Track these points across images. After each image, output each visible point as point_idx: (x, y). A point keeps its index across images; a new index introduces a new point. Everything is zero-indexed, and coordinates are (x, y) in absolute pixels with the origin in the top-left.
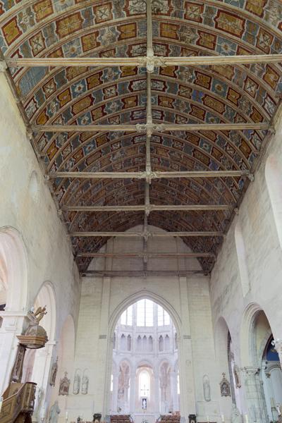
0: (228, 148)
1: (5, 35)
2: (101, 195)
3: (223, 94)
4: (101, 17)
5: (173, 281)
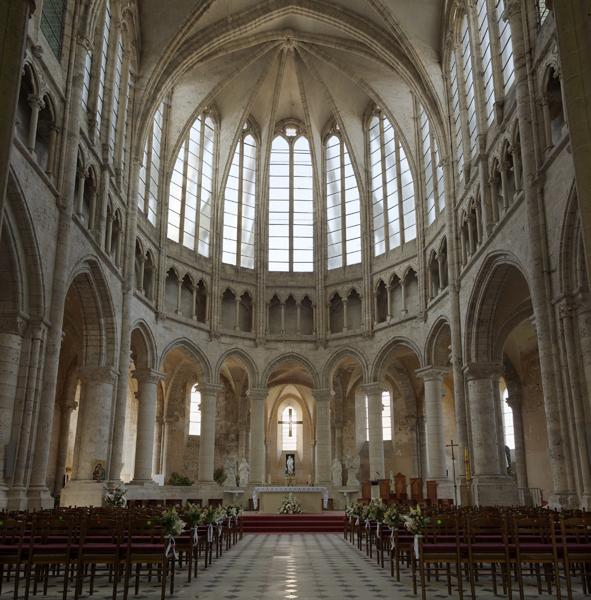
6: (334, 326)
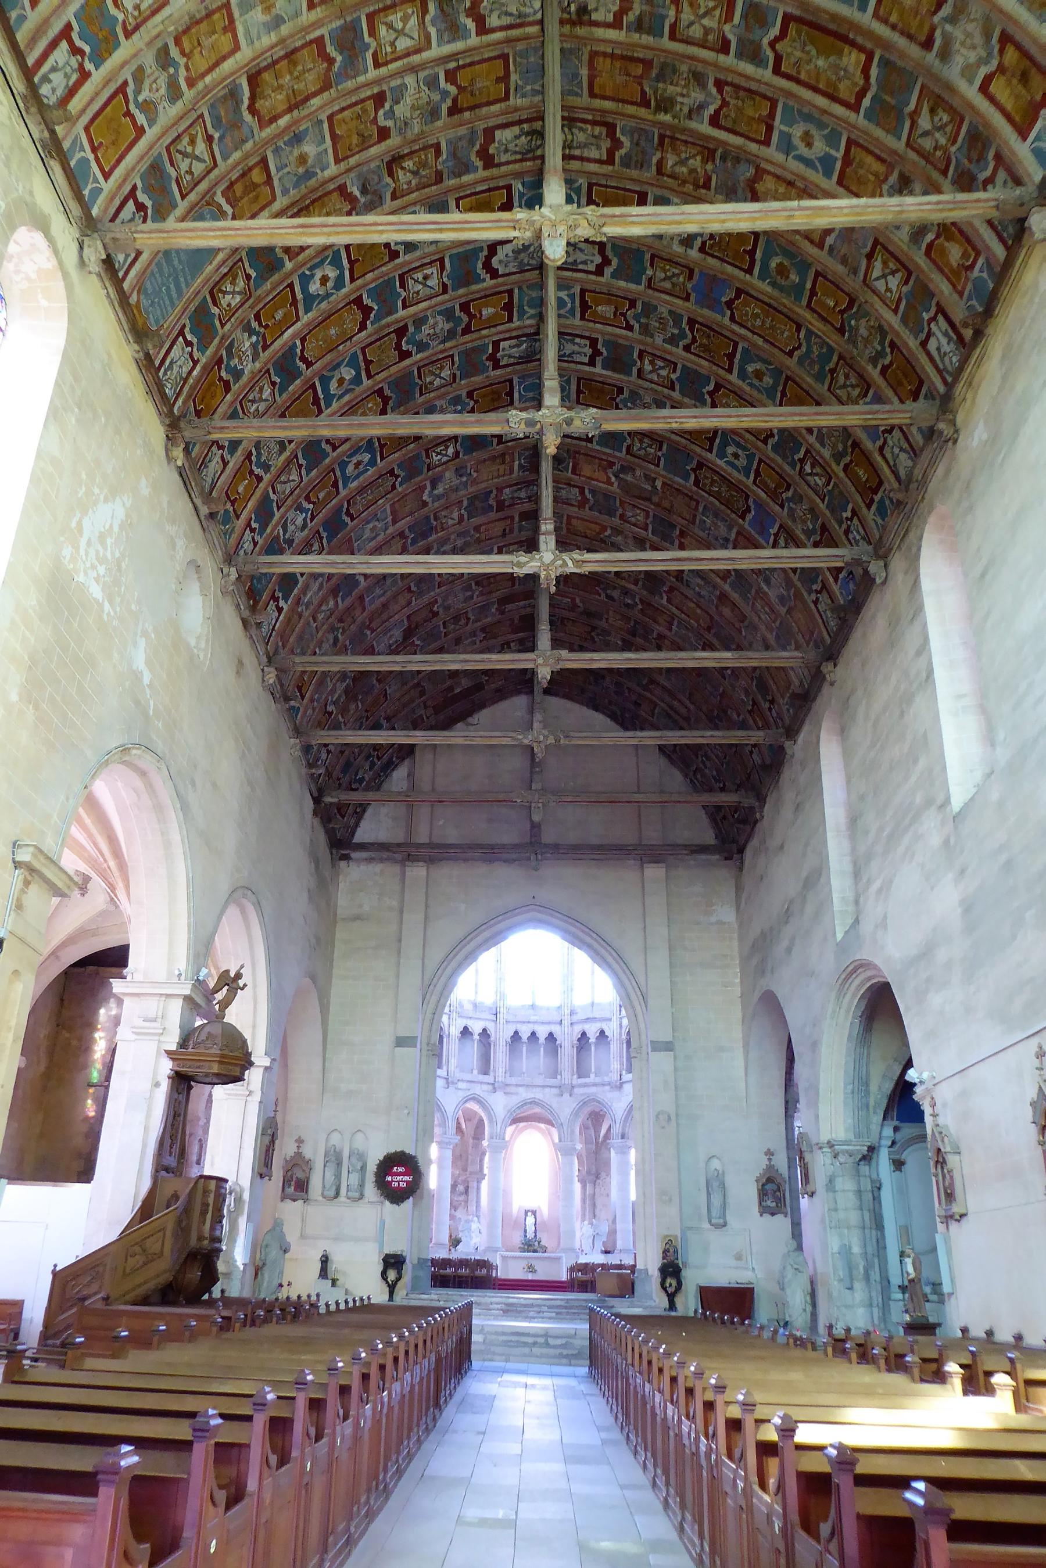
0: (808, 469)
1: (94, 150)
2: (394, 607)
3: (797, 290)
4: (392, 44)
5: (620, 878)
6: (581, 1071)
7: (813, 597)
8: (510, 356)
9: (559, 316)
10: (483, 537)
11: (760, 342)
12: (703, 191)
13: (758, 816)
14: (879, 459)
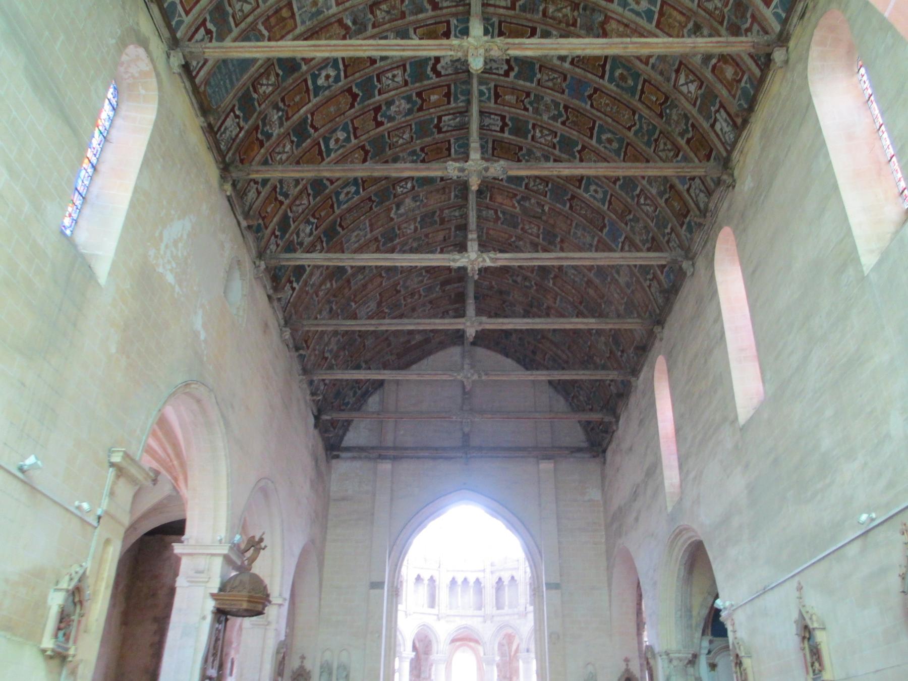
0: (642, 201)
2: (370, 287)
6: (499, 606)
7: (648, 282)
8: (449, 126)
9: (480, 101)
10: (430, 241)
11: (610, 120)
12: (572, 28)
13: (615, 428)
14: (687, 196)
